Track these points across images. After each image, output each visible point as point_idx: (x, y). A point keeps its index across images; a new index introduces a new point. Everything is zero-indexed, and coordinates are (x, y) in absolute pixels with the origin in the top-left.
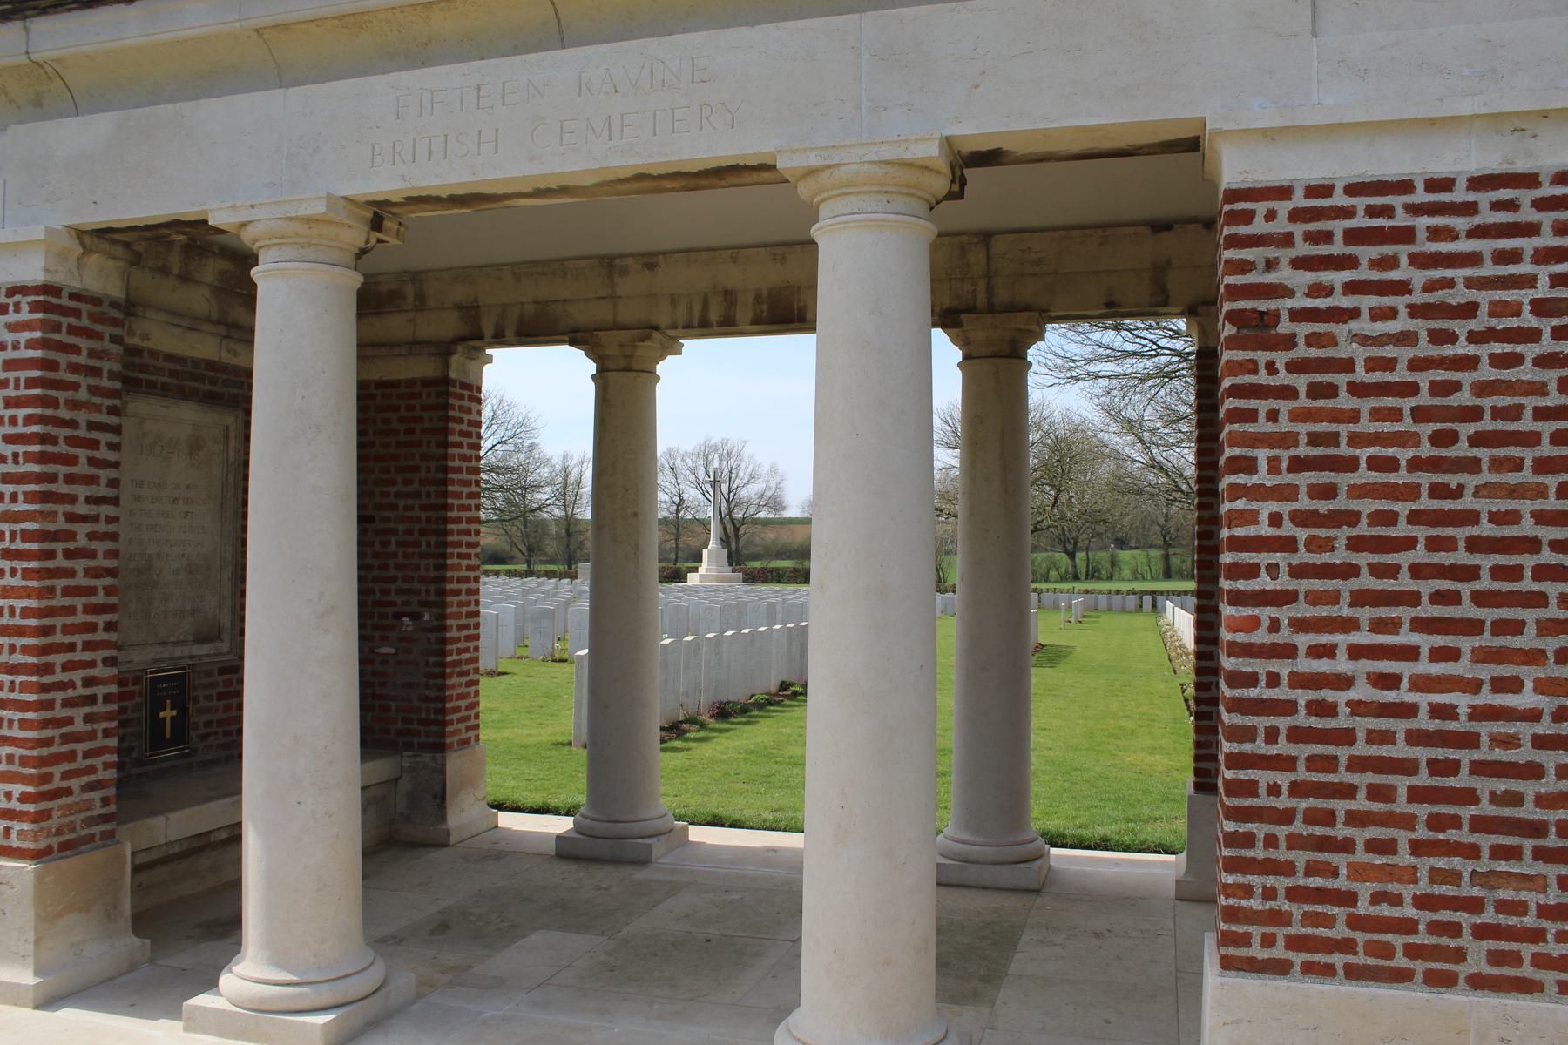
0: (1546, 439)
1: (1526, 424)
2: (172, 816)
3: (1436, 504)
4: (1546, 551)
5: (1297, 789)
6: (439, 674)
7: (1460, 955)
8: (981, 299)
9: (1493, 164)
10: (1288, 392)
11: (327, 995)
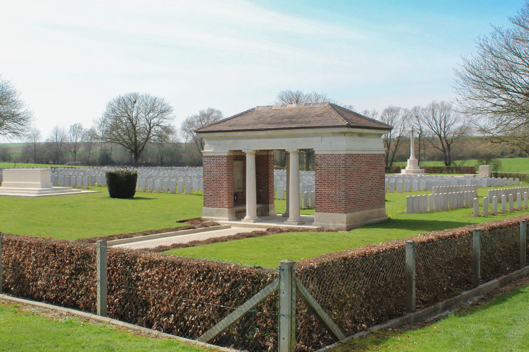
6: (268, 194)
11: (253, 218)
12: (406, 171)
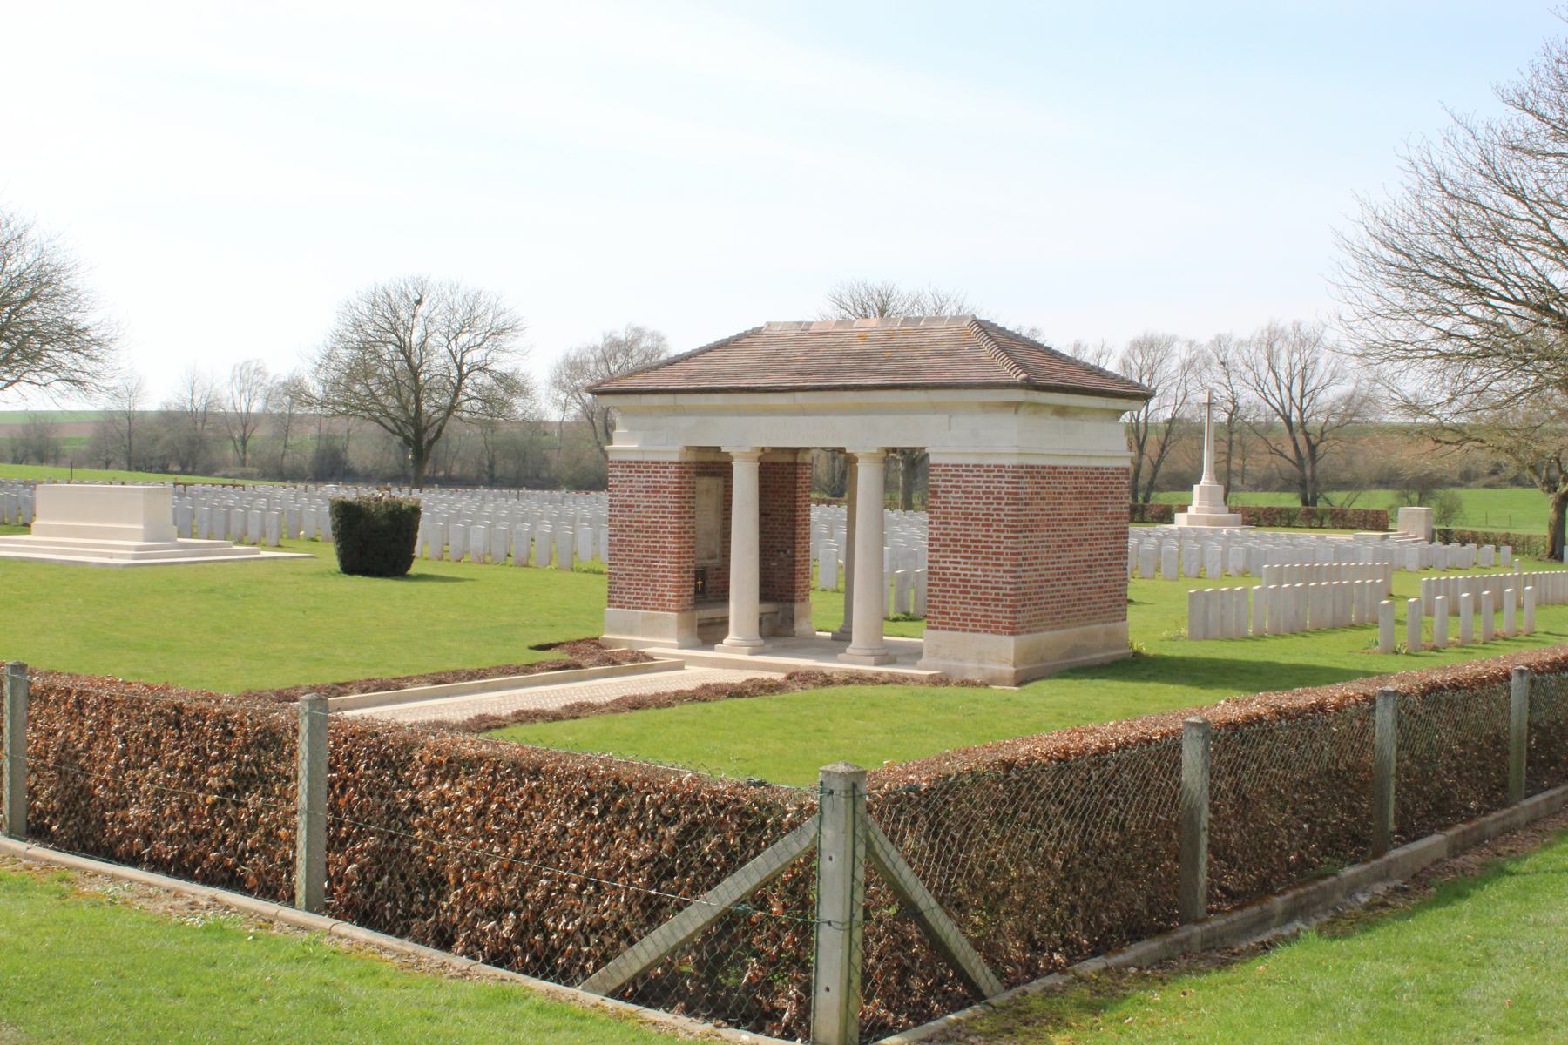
6: (793, 573)
9: (976, 462)
11: (749, 643)
12: (1189, 517)
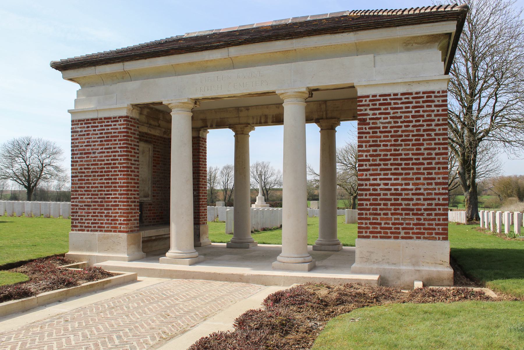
0: (414, 140)
1: (410, 138)
2: (146, 231)
3: (395, 152)
4: (414, 160)
5: (371, 204)
7: (399, 233)
8: (324, 116)
9: (405, 91)
10: (369, 133)
